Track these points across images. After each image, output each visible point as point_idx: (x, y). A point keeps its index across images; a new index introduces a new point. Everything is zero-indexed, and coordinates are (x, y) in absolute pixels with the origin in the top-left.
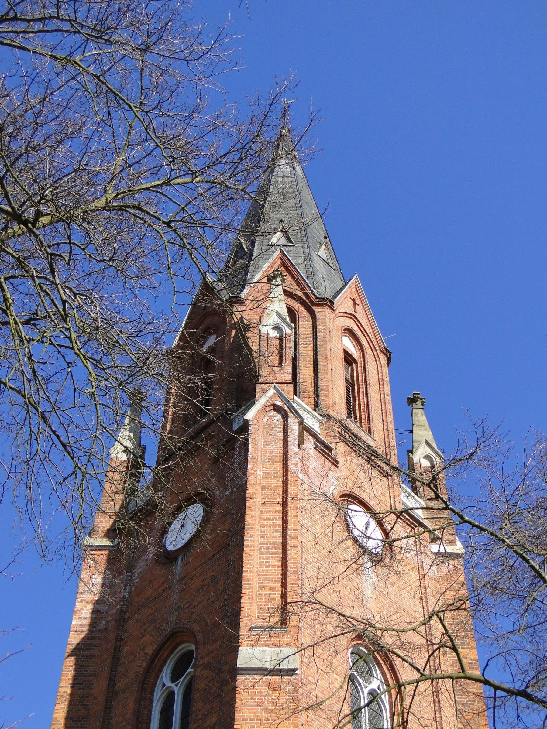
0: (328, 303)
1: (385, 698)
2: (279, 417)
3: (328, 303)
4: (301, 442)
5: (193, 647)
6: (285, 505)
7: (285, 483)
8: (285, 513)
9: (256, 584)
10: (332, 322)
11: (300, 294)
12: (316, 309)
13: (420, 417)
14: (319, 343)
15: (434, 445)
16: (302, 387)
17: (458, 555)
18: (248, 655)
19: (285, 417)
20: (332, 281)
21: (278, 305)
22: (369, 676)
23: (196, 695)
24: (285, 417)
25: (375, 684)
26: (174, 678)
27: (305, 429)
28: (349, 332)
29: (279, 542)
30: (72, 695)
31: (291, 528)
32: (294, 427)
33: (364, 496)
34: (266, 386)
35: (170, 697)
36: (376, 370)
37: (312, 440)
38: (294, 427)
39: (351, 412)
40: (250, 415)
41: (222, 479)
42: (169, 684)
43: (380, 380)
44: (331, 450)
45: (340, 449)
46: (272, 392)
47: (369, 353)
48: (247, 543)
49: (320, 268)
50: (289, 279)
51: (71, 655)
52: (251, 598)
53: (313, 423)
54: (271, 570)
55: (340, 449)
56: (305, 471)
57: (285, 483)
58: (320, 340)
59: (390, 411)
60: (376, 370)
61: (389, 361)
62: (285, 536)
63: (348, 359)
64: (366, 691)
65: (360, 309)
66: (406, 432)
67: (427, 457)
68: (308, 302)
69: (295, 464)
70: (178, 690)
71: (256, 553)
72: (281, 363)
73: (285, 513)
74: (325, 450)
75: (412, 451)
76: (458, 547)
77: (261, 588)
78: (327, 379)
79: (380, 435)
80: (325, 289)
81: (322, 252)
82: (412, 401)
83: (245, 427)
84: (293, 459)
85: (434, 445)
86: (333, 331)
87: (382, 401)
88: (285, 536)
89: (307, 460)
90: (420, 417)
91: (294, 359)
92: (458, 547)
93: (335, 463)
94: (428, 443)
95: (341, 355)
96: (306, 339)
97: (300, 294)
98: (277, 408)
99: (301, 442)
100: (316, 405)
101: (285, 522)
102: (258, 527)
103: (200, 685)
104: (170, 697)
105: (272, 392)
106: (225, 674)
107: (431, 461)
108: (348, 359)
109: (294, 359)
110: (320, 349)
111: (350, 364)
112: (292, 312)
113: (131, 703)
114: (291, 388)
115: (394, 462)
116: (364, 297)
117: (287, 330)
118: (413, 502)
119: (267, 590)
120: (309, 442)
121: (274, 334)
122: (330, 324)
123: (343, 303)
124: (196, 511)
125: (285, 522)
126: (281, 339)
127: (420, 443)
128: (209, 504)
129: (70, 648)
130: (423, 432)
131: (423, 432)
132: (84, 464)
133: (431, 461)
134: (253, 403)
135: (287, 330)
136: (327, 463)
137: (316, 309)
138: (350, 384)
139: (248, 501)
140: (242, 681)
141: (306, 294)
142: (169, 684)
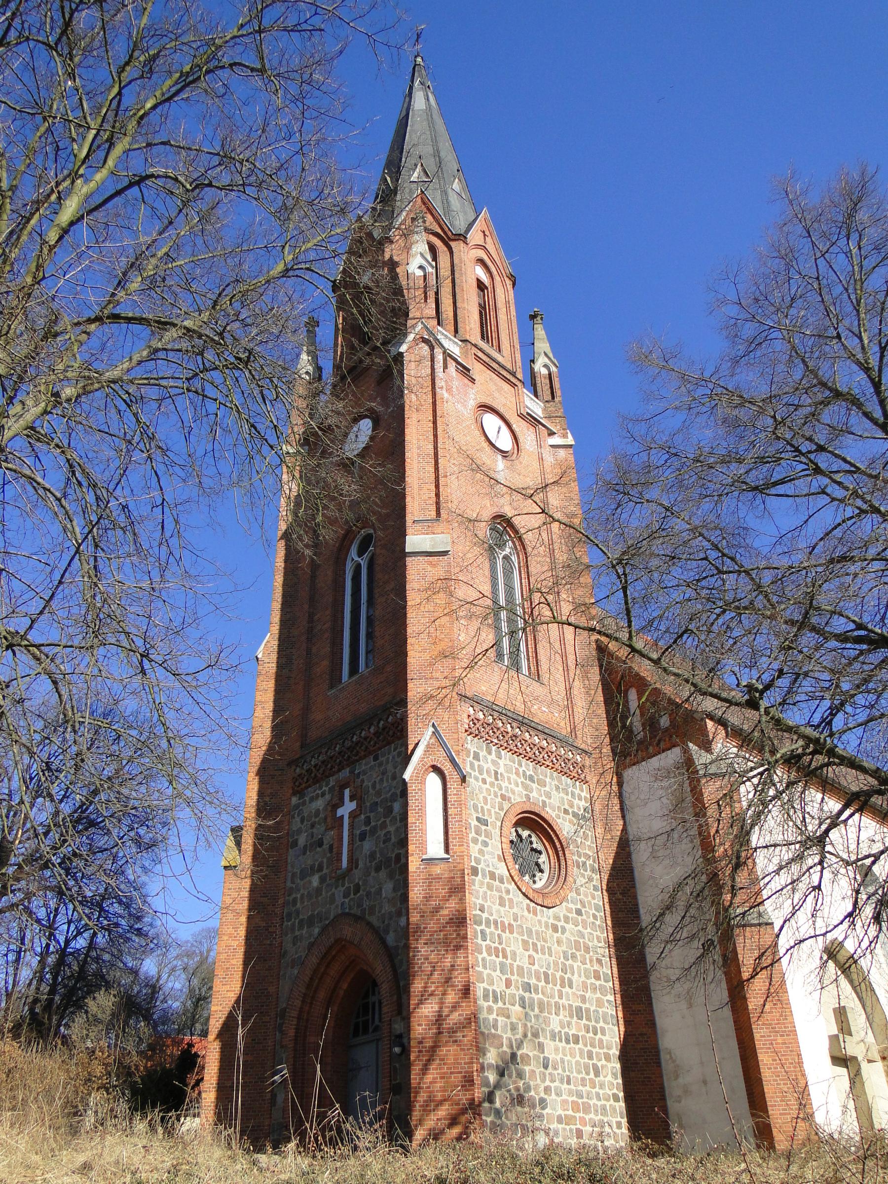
0: (462, 237)
1: (514, 558)
2: (426, 348)
3: (462, 237)
4: (445, 367)
5: (372, 531)
6: (435, 422)
7: (434, 404)
8: (435, 428)
9: (416, 487)
10: (466, 254)
11: (440, 231)
12: (453, 244)
13: (540, 331)
14: (457, 275)
15: (551, 355)
16: (444, 316)
17: (570, 446)
18: (415, 541)
19: (432, 348)
20: (465, 213)
21: (420, 247)
22: (502, 546)
23: (377, 568)
24: (432, 348)
25: (507, 551)
26: (360, 554)
27: (447, 355)
28: (481, 261)
29: (432, 452)
30: (285, 568)
31: (440, 440)
32: (439, 357)
33: (495, 405)
34: (415, 321)
35: (358, 567)
36: (504, 294)
37: (454, 364)
38: (439, 357)
39: (484, 336)
40: (403, 348)
41: (385, 402)
42: (356, 558)
43: (507, 303)
44: (468, 370)
45: (477, 370)
46: (420, 326)
47: (497, 279)
48: (408, 455)
49: (454, 199)
50: (429, 217)
51: (281, 538)
52: (413, 498)
53: (455, 349)
54: (427, 475)
55: (477, 370)
56: (449, 390)
57: (434, 404)
58: (456, 266)
59: (515, 330)
60: (504, 294)
61: (514, 285)
62: (436, 448)
63: (481, 286)
64: (501, 557)
65: (489, 239)
66: (528, 345)
67: (545, 366)
68: (448, 238)
69: (442, 388)
70: (363, 562)
71: (415, 462)
72: (426, 301)
73: (435, 428)
74: (465, 371)
75: (533, 361)
76: (570, 440)
77: (420, 489)
78: (464, 309)
79: (508, 354)
80: (459, 225)
81: (456, 185)
82: (533, 317)
83: (399, 358)
84: (439, 383)
85: (551, 355)
86: (468, 263)
87: (509, 321)
88: (436, 448)
89: (449, 377)
90: (540, 331)
91: (437, 293)
92: (570, 440)
93: (473, 381)
94: (546, 354)
95: (475, 284)
96: (445, 272)
97: (440, 231)
98: (425, 341)
99: (445, 367)
100: (456, 331)
101: (435, 436)
102: (415, 442)
103: (379, 561)
104: (358, 567)
105: (420, 326)
106: (398, 556)
107: (549, 369)
108: (481, 286)
109: (437, 293)
110: (457, 281)
111: (483, 291)
112: (432, 249)
113: (329, 573)
114: (435, 322)
115: (520, 376)
116: (492, 228)
117: (430, 270)
118: (537, 408)
119: (425, 491)
120: (452, 365)
121: (420, 273)
122: (464, 257)
123: (475, 236)
124: (366, 425)
125: (435, 436)
126: (425, 276)
127: (539, 354)
128: (377, 423)
129: (280, 534)
130: (542, 345)
131: (542, 345)
132: (273, 383)
133: (549, 369)
134: (405, 335)
135: (430, 270)
136: (466, 381)
137: (453, 244)
138: (483, 308)
139: (407, 421)
140: (409, 560)
141: (445, 233)
142: (356, 558)
